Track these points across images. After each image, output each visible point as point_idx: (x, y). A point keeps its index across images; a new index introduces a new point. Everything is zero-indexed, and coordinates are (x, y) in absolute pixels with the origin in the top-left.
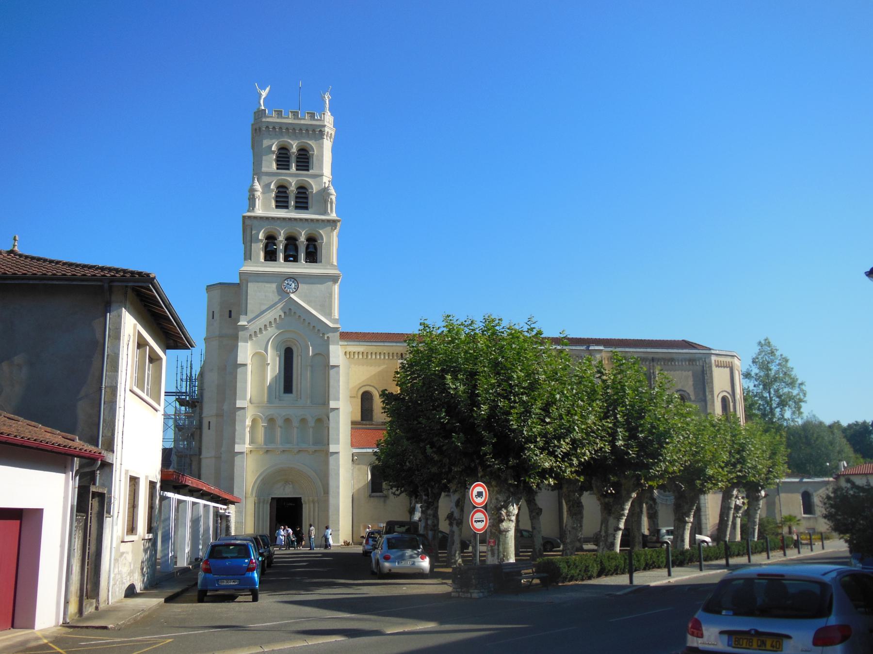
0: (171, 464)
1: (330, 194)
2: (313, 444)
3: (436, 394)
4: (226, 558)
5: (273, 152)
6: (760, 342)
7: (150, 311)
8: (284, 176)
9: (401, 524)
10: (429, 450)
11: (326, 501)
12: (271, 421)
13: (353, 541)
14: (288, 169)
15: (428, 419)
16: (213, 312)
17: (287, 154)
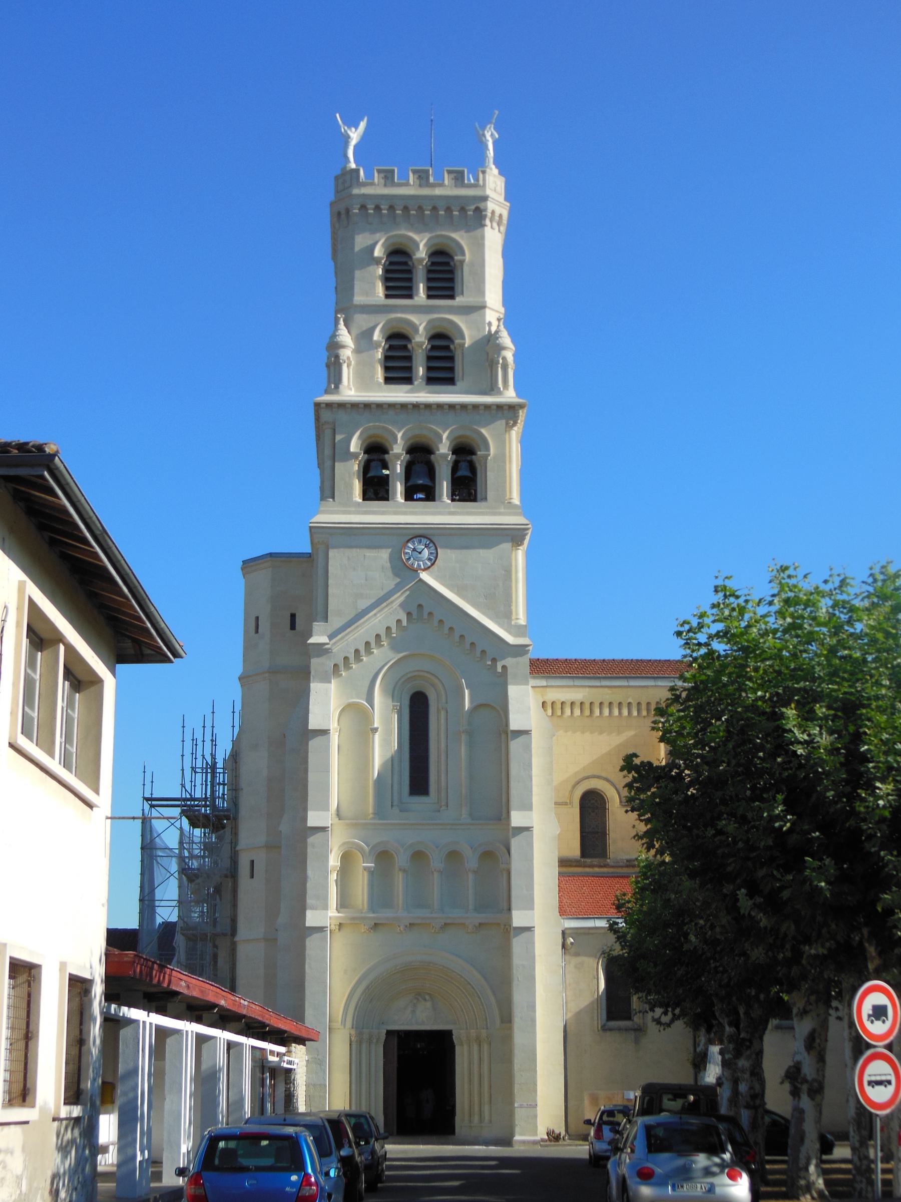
0: (174, 955)
1: (501, 348)
2: (477, 910)
3: (759, 758)
4: (244, 1169)
5: (377, 261)
7: (64, 557)
8: (402, 312)
9: (678, 1092)
10: (745, 903)
11: (507, 1039)
12: (383, 857)
13: (567, 1131)
14: (410, 297)
15: (743, 820)
16: (257, 618)
17: (406, 264)
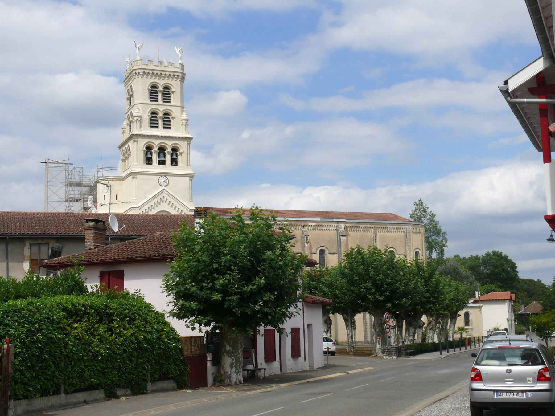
6: (415, 203)
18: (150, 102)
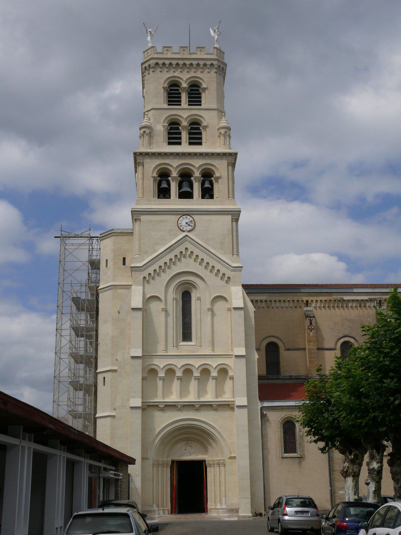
18: (166, 106)
